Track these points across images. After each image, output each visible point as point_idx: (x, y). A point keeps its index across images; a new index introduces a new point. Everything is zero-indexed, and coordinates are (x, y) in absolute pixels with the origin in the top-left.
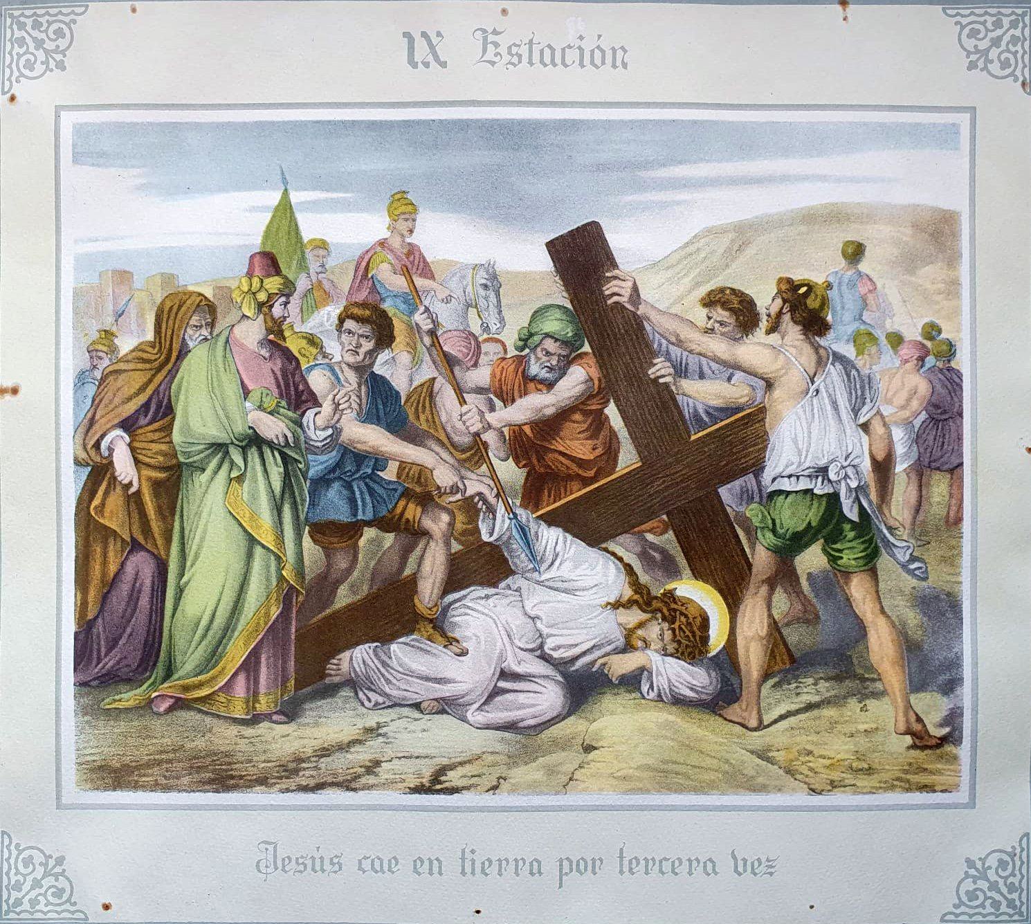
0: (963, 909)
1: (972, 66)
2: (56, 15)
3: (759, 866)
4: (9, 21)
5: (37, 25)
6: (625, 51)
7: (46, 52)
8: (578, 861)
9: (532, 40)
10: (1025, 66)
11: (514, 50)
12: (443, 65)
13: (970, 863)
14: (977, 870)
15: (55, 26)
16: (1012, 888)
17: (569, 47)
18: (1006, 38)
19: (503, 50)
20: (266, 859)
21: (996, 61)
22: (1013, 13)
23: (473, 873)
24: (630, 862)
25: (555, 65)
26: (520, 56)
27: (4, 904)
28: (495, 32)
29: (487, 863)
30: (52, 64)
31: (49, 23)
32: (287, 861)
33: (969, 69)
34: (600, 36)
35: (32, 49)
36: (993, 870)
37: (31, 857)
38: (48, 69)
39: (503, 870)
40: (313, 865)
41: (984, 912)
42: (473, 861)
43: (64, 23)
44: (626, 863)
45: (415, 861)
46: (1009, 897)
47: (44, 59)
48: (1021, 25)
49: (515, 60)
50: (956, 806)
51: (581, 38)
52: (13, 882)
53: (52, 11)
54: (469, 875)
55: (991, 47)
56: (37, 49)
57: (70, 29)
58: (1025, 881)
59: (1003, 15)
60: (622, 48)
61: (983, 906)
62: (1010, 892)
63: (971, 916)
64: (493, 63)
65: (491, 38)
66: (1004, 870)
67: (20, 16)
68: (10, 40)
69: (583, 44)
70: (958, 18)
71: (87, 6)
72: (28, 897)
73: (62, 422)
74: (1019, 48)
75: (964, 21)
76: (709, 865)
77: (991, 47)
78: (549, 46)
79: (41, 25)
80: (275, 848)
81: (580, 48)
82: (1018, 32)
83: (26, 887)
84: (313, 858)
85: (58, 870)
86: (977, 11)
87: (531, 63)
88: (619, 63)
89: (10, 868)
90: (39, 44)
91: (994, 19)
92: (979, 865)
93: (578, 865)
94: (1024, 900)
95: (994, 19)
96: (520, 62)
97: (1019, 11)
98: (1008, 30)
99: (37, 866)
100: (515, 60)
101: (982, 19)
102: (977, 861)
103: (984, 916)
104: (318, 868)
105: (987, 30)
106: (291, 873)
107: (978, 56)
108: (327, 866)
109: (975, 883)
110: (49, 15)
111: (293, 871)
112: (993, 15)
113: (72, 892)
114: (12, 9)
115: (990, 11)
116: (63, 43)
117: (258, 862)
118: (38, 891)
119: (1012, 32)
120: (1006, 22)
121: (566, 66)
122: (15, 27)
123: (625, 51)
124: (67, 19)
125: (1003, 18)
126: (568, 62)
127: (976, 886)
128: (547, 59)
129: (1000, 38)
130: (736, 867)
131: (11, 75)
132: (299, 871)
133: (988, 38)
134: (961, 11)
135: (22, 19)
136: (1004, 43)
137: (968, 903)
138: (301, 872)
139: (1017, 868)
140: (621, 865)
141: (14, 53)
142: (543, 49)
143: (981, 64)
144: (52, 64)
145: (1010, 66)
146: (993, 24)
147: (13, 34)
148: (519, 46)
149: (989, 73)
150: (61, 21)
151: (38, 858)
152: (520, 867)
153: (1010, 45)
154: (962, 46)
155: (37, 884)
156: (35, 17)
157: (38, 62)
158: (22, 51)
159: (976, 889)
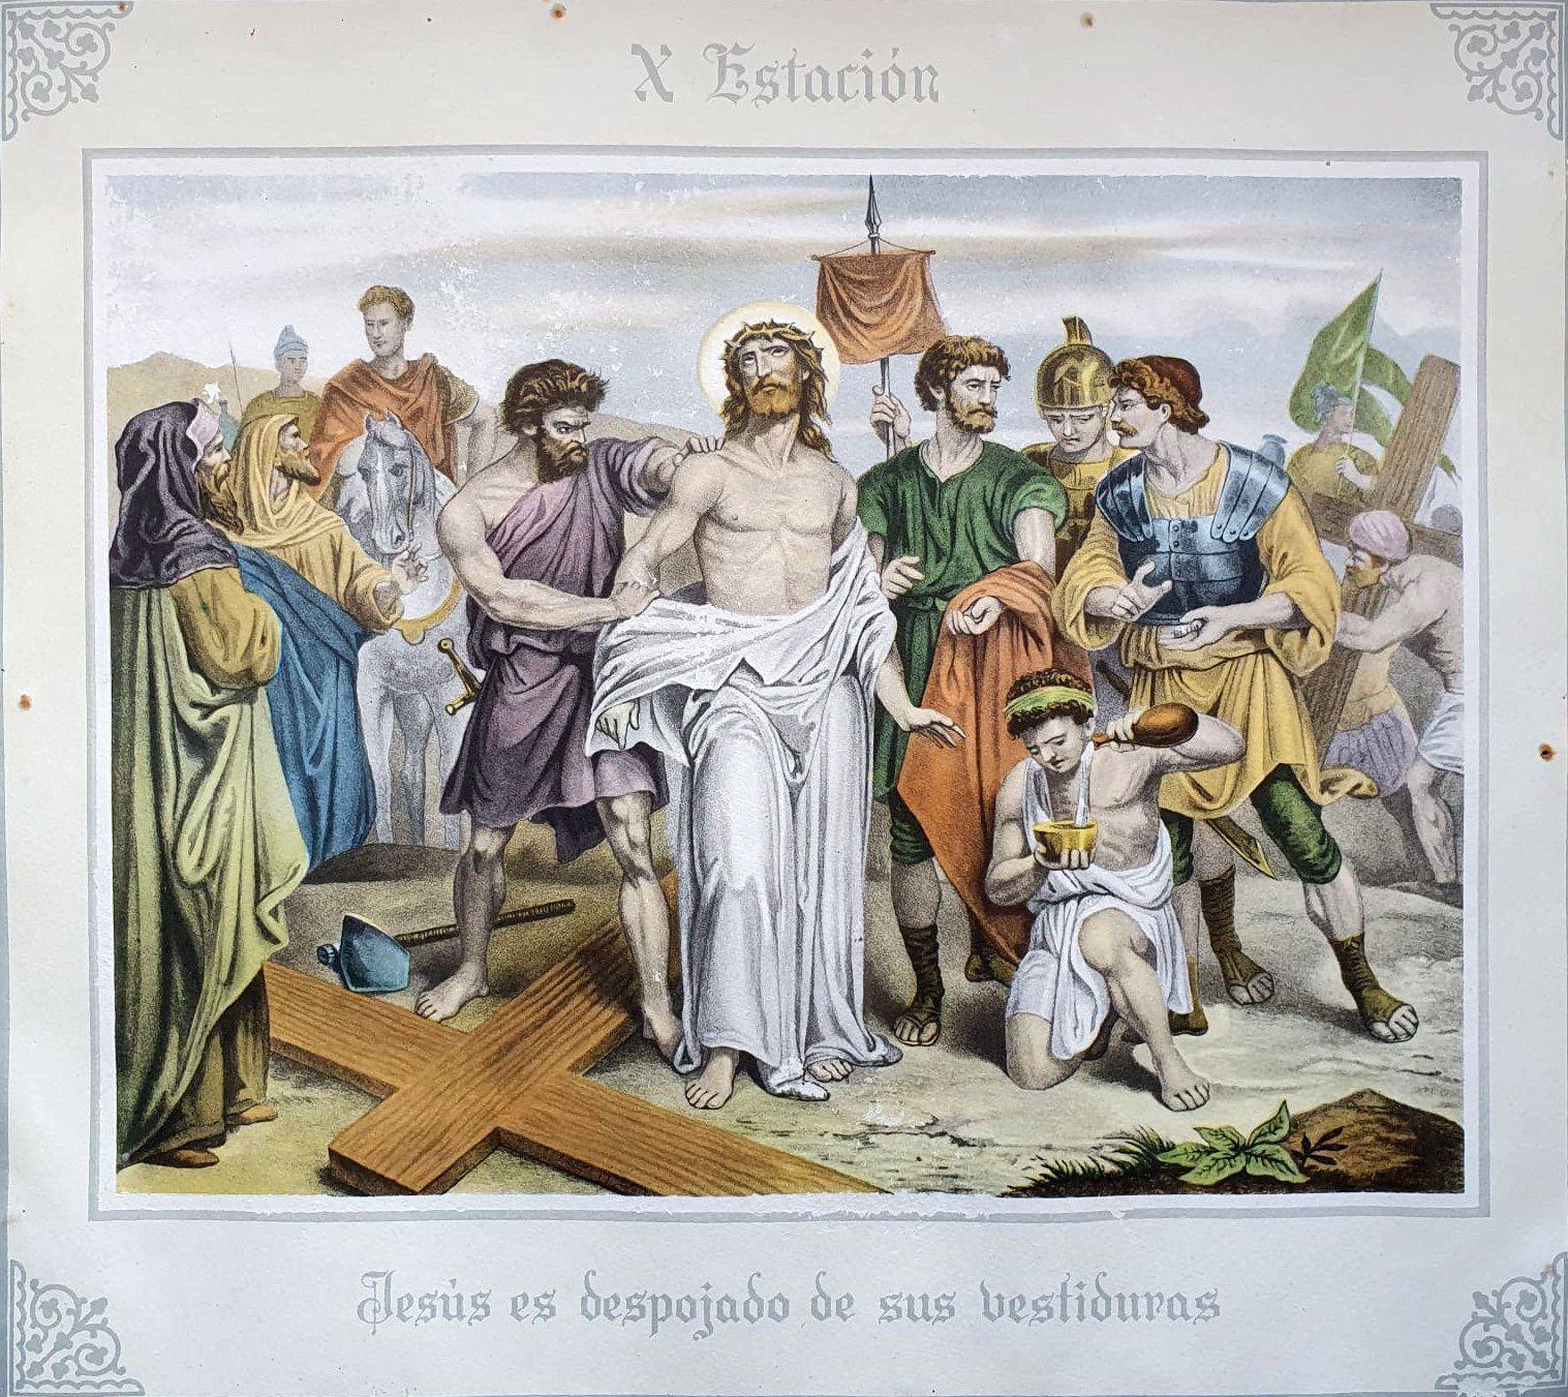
0: (30, 1294)
1: (1475, 93)
3: (849, 1306)
7: (67, 72)
12: (668, 97)
14: (1490, 1309)
15: (80, 32)
16: (1541, 1335)
17: (850, 68)
19: (749, 77)
22: (1535, 14)
28: (737, 50)
29: (406, 1301)
30: (76, 91)
33: (1471, 98)
34: (895, 51)
35: (44, 67)
42: (1081, 1299)
43: (95, 28)
46: (1538, 1348)
47: (63, 84)
48: (1546, 33)
49: (769, 91)
50: (1464, 1213)
52: (28, 1338)
55: (1500, 68)
56: (51, 66)
57: (104, 37)
59: (14, 48)
60: (930, 68)
62: (1538, 1341)
64: (734, 98)
65: (731, 59)
67: (23, 17)
70: (1455, 21)
75: (1464, 25)
76: (1177, 1304)
77: (1500, 68)
78: (819, 69)
79: (58, 29)
81: (865, 69)
83: (47, 1347)
84: (445, 1297)
87: (792, 96)
88: (925, 92)
89: (24, 1318)
90: (55, 59)
91: (1508, 23)
92: (1493, 1302)
95: (1508, 23)
97: (1544, 12)
98: (1527, 41)
102: (1491, 1297)
104: (918, 1312)
106: (619, 1320)
107: (1484, 78)
108: (468, 1310)
109: (1486, 1329)
112: (1507, 18)
113: (118, 1347)
116: (92, 60)
117: (361, 1307)
118: (65, 1352)
119: (1533, 43)
120: (1524, 28)
121: (846, 99)
122: (18, 32)
123: (934, 74)
124: (100, 23)
128: (817, 90)
129: (1515, 52)
130: (987, 1306)
132: (1203, 1318)
133: (1498, 53)
135: (28, 21)
136: (1520, 61)
141: (18, 74)
142: (886, 73)
143: (1488, 91)
144: (76, 91)
147: (1524, 18)
149: (99, 68)
150: (88, 25)
152: (1155, 1308)
155: (63, 1342)
156: (47, 18)
157: (54, 88)
158: (29, 70)
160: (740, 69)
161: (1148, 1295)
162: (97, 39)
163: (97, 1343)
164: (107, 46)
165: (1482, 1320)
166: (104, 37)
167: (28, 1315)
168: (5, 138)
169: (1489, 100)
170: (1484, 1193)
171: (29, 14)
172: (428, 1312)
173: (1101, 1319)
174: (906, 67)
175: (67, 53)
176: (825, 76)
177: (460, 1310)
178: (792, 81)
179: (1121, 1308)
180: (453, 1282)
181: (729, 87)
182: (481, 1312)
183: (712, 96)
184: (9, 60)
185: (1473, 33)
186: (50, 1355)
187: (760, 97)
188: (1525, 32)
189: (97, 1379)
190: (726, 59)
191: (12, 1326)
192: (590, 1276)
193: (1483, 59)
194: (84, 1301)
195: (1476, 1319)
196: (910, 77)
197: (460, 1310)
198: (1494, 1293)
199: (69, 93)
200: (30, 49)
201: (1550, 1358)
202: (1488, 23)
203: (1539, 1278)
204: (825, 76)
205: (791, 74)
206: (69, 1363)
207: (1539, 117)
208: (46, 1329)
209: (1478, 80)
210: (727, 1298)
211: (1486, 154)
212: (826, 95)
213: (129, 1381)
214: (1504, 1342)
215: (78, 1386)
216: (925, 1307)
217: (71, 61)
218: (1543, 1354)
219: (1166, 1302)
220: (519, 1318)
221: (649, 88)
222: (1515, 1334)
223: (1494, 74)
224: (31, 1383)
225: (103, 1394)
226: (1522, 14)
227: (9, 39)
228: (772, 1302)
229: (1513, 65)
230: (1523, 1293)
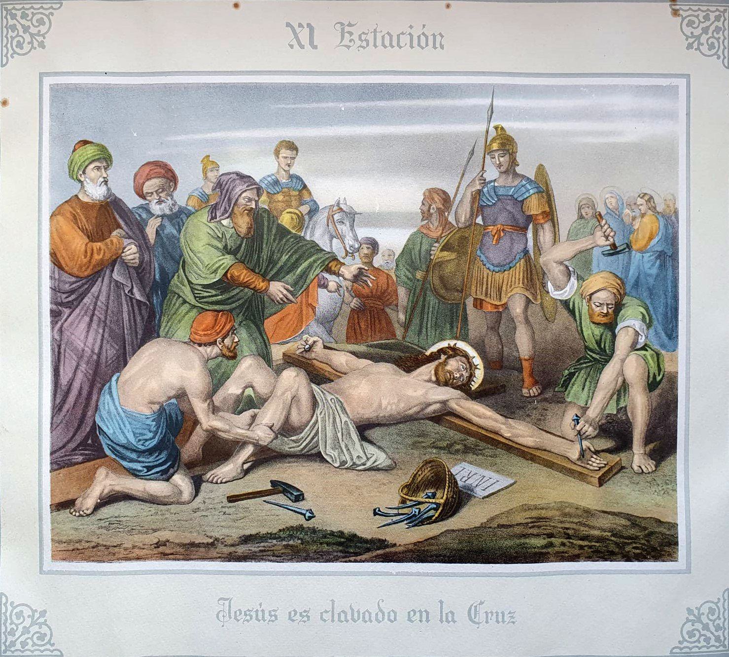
0: (10, 608)
2: (39, 9)
5: (24, 16)
6: (442, 36)
7: (32, 35)
8: (389, 613)
10: (725, 48)
11: (363, 37)
13: (690, 611)
14: (694, 615)
17: (403, 33)
18: (712, 28)
19: (355, 37)
21: (705, 44)
22: (717, 10)
24: (339, 614)
25: (392, 47)
26: (367, 41)
27: (727, 18)
28: (350, 25)
30: (36, 44)
31: (34, 15)
33: (688, 48)
34: (424, 26)
35: (21, 33)
36: (705, 616)
37: (22, 612)
40: (257, 616)
41: (699, 645)
44: (444, 615)
45: (409, 613)
46: (716, 634)
48: (722, 19)
49: (364, 44)
51: (411, 27)
52: (9, 630)
54: (444, 622)
55: (701, 34)
56: (29, 632)
60: (440, 34)
62: (717, 631)
64: (348, 47)
65: (347, 29)
68: (708, 10)
69: (412, 31)
73: (44, 402)
77: (701, 34)
78: (388, 33)
79: (28, 15)
80: (230, 603)
81: (410, 34)
82: (720, 24)
85: (42, 620)
87: (375, 46)
88: (438, 45)
89: (6, 619)
90: (26, 29)
91: (705, 14)
92: (696, 612)
93: (389, 616)
95: (705, 14)
97: (722, 9)
98: (713, 23)
100: (364, 44)
103: (700, 648)
104: (260, 617)
110: (34, 9)
111: (242, 620)
116: (43, 29)
117: (219, 613)
118: (26, 636)
119: (716, 23)
120: (712, 16)
121: (400, 47)
122: (9, 17)
123: (442, 36)
124: (47, 12)
125: (710, 13)
126: (402, 45)
127: (694, 627)
128: (387, 43)
131: (7, 53)
134: (701, 8)
135: (14, 11)
137: (689, 640)
138: (273, 621)
139: (721, 613)
140: (441, 616)
141: (9, 36)
143: (695, 45)
144: (36, 44)
145: (714, 48)
146: (704, 17)
147: (7, 22)
148: (367, 34)
150: (42, 13)
151: (27, 612)
152: (489, 618)
154: (683, 32)
155: (26, 630)
158: (14, 35)
159: (694, 630)
160: (351, 34)
162: (46, 19)
165: (691, 621)
167: (9, 618)
168: (3, 66)
169: (696, 49)
170: (50, 572)
171: (14, 8)
172: (248, 618)
174: (429, 33)
175: (31, 26)
176: (391, 36)
177: (263, 617)
178: (375, 39)
180: (260, 605)
181: (346, 42)
182: (273, 618)
184: (5, 30)
185: (689, 18)
188: (712, 18)
189: (42, 648)
190: (344, 29)
194: (36, 611)
195: (688, 620)
196: (431, 39)
197: (263, 617)
198: (696, 608)
199: (32, 46)
200: (15, 25)
201: (722, 638)
202: (696, 14)
204: (391, 36)
207: (719, 58)
208: (17, 626)
209: (691, 40)
210: (367, 611)
211: (689, 75)
213: (55, 650)
214: (701, 631)
215: (32, 652)
217: (33, 30)
218: (719, 636)
220: (412, 622)
221: (294, 42)
222: (706, 627)
223: (698, 38)
224: (11, 651)
225: (35, 656)
226: (694, 9)
227: (5, 20)
229: (707, 34)
230: (710, 608)
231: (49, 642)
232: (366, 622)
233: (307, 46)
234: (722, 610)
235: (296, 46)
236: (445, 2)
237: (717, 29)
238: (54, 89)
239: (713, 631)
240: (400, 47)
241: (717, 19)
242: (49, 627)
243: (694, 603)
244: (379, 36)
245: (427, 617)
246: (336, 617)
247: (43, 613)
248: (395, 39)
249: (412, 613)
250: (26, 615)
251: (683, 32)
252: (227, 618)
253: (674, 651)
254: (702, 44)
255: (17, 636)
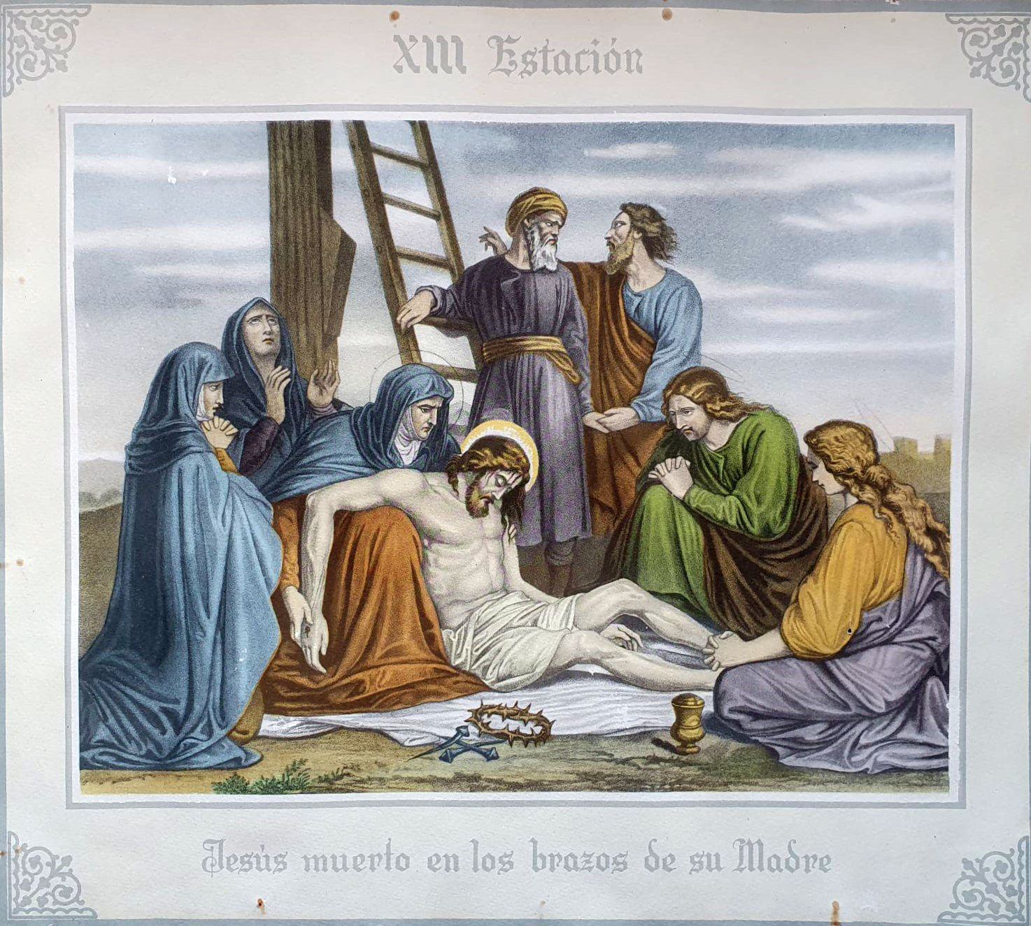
1: (975, 73)
4: (8, 19)
5: (37, 24)
7: (46, 51)
9: (546, 47)
11: (529, 58)
17: (584, 52)
18: (1009, 46)
19: (518, 58)
20: (212, 857)
21: (57, 43)
22: (1016, 20)
23: (325, 870)
26: (535, 65)
28: (510, 40)
30: (53, 65)
32: (232, 860)
34: (614, 40)
38: (49, 70)
39: (376, 865)
46: (1008, 900)
48: (1023, 33)
49: (530, 68)
51: (595, 42)
53: (53, 10)
55: (993, 55)
57: (73, 30)
58: (1024, 884)
60: (637, 52)
61: (980, 907)
62: (1009, 895)
63: (969, 916)
64: (508, 72)
65: (506, 46)
66: (1003, 872)
69: (597, 49)
70: (962, 25)
71: (89, 8)
72: (36, 897)
74: (1021, 55)
75: (967, 28)
77: (993, 55)
78: (563, 53)
79: (41, 23)
83: (34, 887)
84: (257, 857)
86: (980, 18)
88: (633, 67)
89: (53, 15)
90: (40, 44)
92: (977, 866)
94: (1024, 903)
95: (997, 26)
96: (535, 69)
97: (1021, 19)
98: (1009, 39)
99: (44, 866)
101: (985, 26)
102: (974, 862)
103: (983, 917)
105: (990, 38)
107: (981, 63)
108: (273, 865)
114: (10, 8)
115: (993, 18)
116: (64, 44)
117: (205, 861)
119: (1014, 39)
120: (1008, 30)
121: (580, 72)
123: (640, 54)
126: (583, 67)
127: (973, 887)
128: (562, 67)
135: (21, 18)
136: (1006, 51)
137: (965, 904)
141: (14, 53)
143: (983, 71)
147: (1020, 899)
149: (991, 79)
152: (555, 863)
153: (1012, 53)
154: (965, 52)
155: (44, 882)
157: (39, 62)
161: (806, 857)
163: (66, 884)
164: (74, 35)
166: (73, 30)
172: (247, 866)
173: (603, 870)
177: (267, 864)
179: (335, 864)
180: (263, 847)
181: (505, 64)
182: (281, 866)
183: (493, 70)
185: (974, 33)
186: (34, 893)
187: (525, 71)
190: (501, 44)
191: (10, 874)
192: (653, 843)
193: (981, 50)
194: (58, 857)
196: (624, 58)
198: (977, 860)
199: (48, 65)
203: (1009, 853)
204: (567, 57)
205: (545, 58)
206: (48, 897)
209: (976, 64)
212: (568, 70)
216: (258, 863)
218: (1012, 904)
219: (818, 861)
221: (404, 62)
228: (544, 867)
229: (1001, 54)
231: (76, 899)
232: (261, 870)
233: (424, 69)
234: (1017, 867)
235: (406, 68)
236: (661, 10)
237: (1016, 47)
238: (78, 128)
239: (1004, 895)
240: (580, 72)
241: (1015, 32)
242: (75, 879)
243: (975, 851)
244: (550, 56)
245: (456, 863)
246: (393, 861)
247: (67, 860)
248: (573, 61)
249: (359, 860)
250: (999, 71)
251: (965, 52)
252: (217, 867)
253: (944, 918)
254: (994, 69)
255: (32, 891)
